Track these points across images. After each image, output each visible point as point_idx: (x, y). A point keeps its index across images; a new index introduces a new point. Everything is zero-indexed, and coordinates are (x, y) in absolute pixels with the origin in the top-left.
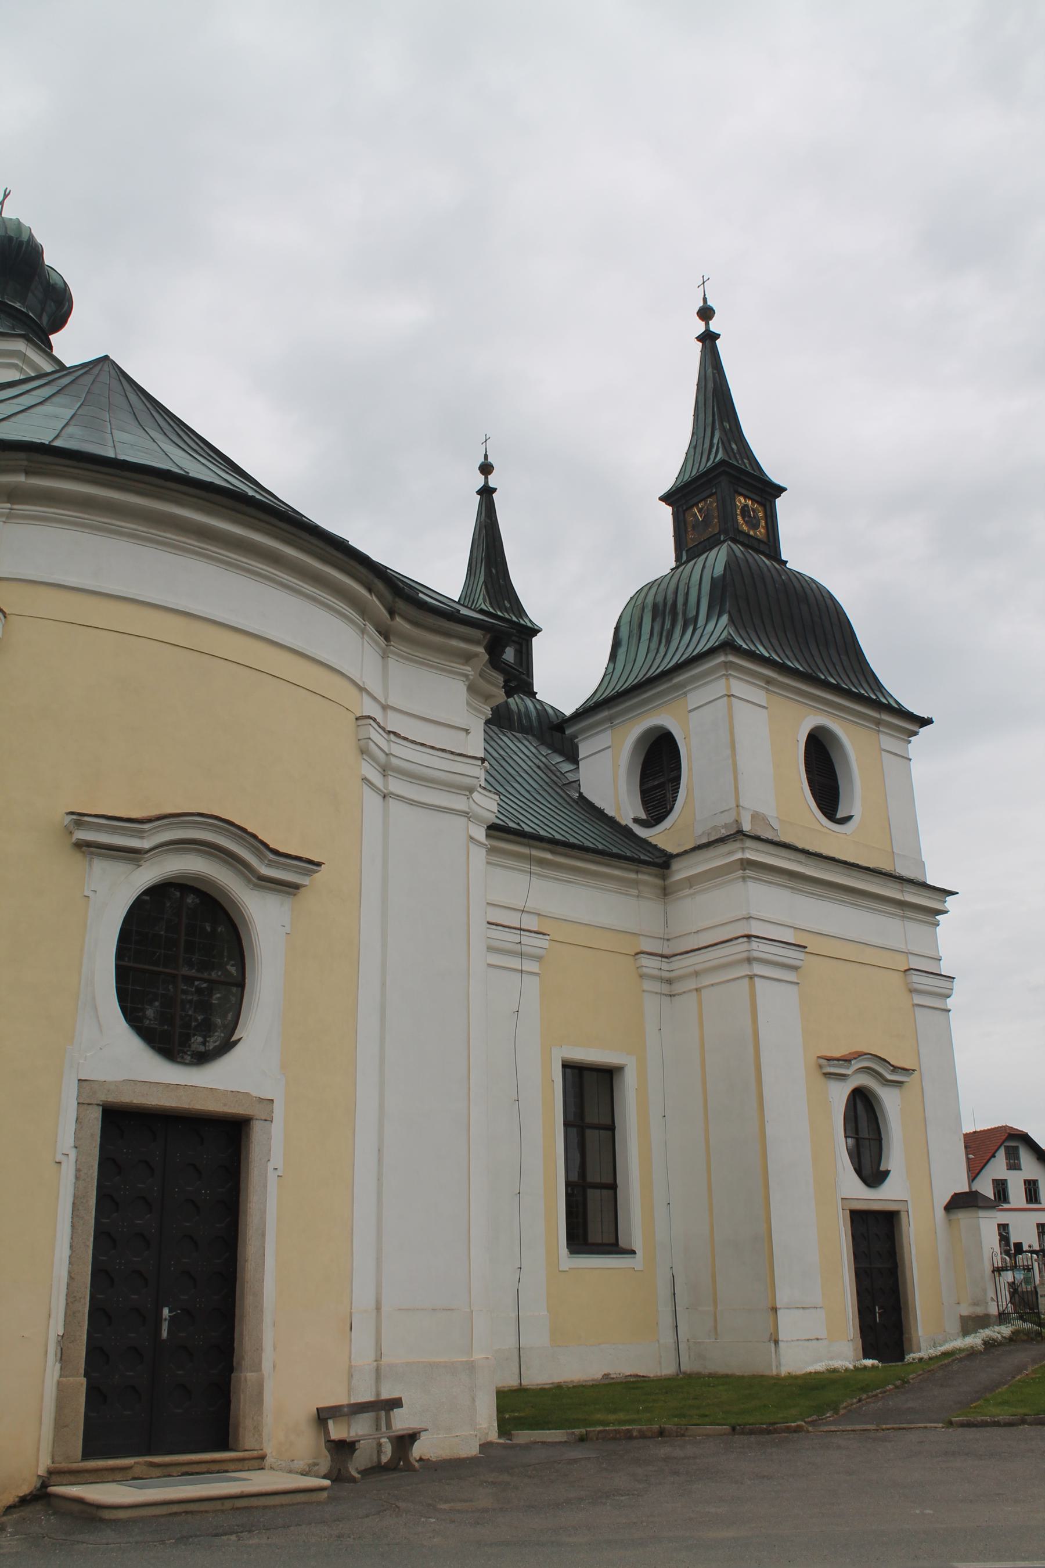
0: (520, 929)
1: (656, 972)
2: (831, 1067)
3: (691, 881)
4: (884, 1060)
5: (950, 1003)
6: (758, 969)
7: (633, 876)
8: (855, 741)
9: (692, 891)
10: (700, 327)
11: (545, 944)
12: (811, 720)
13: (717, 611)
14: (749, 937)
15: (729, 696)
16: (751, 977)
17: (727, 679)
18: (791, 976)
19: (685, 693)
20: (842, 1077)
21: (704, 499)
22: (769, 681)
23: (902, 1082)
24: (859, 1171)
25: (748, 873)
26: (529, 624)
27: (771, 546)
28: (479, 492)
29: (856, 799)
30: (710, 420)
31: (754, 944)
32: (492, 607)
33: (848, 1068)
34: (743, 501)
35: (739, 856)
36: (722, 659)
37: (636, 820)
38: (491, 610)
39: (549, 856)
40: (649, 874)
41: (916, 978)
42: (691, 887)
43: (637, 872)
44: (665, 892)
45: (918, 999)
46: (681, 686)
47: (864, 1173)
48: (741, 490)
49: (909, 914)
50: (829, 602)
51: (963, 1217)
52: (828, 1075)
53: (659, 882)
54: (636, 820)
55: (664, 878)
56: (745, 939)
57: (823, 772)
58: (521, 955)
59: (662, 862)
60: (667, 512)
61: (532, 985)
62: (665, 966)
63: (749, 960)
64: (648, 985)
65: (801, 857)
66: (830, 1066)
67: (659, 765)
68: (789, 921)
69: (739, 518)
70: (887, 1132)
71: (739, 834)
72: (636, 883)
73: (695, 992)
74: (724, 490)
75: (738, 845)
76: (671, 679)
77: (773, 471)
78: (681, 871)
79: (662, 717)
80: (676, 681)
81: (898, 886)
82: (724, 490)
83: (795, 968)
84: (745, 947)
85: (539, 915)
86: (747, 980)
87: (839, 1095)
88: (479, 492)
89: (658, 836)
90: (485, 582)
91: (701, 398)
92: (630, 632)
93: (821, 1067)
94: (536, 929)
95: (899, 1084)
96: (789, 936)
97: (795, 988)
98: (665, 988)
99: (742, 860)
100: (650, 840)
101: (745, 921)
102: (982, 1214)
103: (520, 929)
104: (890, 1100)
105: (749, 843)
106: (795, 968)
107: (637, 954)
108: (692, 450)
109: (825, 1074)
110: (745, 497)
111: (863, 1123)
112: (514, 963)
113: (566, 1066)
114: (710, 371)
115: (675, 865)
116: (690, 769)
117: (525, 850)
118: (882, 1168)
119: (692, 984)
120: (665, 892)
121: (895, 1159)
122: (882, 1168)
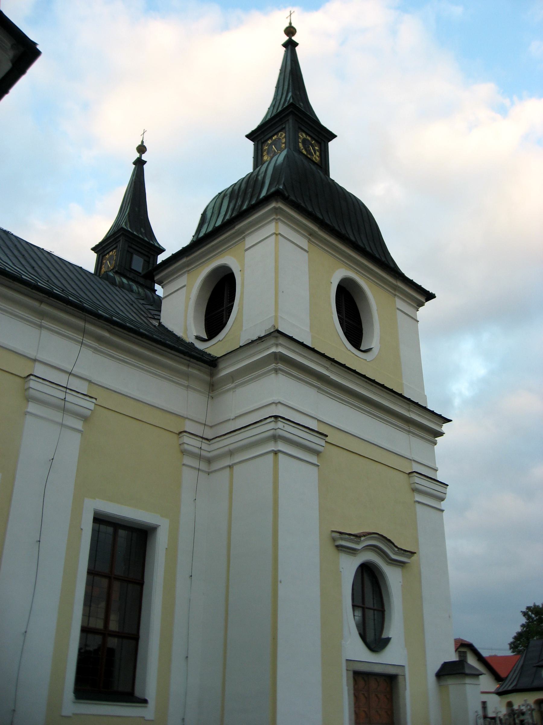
0: (66, 388)
1: (196, 451)
2: (342, 542)
3: (232, 377)
4: (389, 541)
5: (443, 505)
6: (281, 446)
7: (184, 368)
8: (376, 298)
9: (233, 385)
10: (286, 38)
11: (92, 406)
12: (341, 273)
13: (276, 183)
14: (276, 417)
15: (277, 235)
16: (276, 453)
17: (277, 223)
18: (313, 459)
19: (244, 238)
20: (353, 551)
21: (276, 134)
22: (312, 234)
23: (404, 563)
24: (363, 636)
25: (280, 366)
26: (156, 244)
27: (324, 164)
28: (135, 163)
29: (374, 338)
30: (286, 87)
31: (280, 425)
32: (131, 228)
33: (358, 543)
34: (304, 136)
35: (274, 350)
36: (273, 205)
37: (198, 338)
38: (129, 230)
39: (106, 334)
40: (199, 370)
41: (417, 479)
42: (233, 382)
43: (188, 366)
44: (213, 388)
45: (418, 498)
46: (241, 232)
47: (368, 640)
48: (303, 128)
49: (412, 429)
50: (362, 207)
51: (452, 684)
52: (339, 548)
53: (207, 378)
54: (198, 338)
55: (212, 375)
56: (273, 419)
57: (350, 308)
58: (64, 410)
59: (211, 363)
60: (250, 145)
61: (72, 444)
62: (205, 446)
63: (275, 438)
64: (187, 460)
65: (328, 364)
66: (342, 539)
67: (220, 297)
68: (313, 413)
69: (301, 145)
70: (390, 605)
71: (277, 334)
72: (187, 376)
73: (228, 469)
74: (292, 125)
75: (273, 341)
76: (234, 227)
77: (326, 120)
78: (226, 370)
79: (228, 260)
80: (237, 227)
81: (406, 406)
82: (292, 125)
83: (317, 453)
84: (272, 425)
85: (90, 382)
86: (271, 456)
87: (349, 567)
88: (135, 163)
89: (215, 348)
90: (128, 214)
91: (282, 77)
92: (213, 213)
93: (334, 540)
94: (85, 393)
95: (401, 564)
96: (313, 425)
97: (316, 469)
98: (203, 466)
99: (275, 354)
100: (206, 350)
101: (274, 405)
102: (468, 680)
103: (66, 388)
104: (393, 577)
105: (281, 340)
106: (317, 453)
107: (181, 433)
108: (272, 108)
109: (337, 546)
110: (307, 134)
111: (370, 602)
112: (57, 416)
113: (100, 520)
114: (289, 63)
115: (221, 365)
116: (242, 293)
117: (81, 323)
118: (384, 636)
119: (227, 462)
120: (213, 388)
121: (395, 628)
122: (384, 636)
